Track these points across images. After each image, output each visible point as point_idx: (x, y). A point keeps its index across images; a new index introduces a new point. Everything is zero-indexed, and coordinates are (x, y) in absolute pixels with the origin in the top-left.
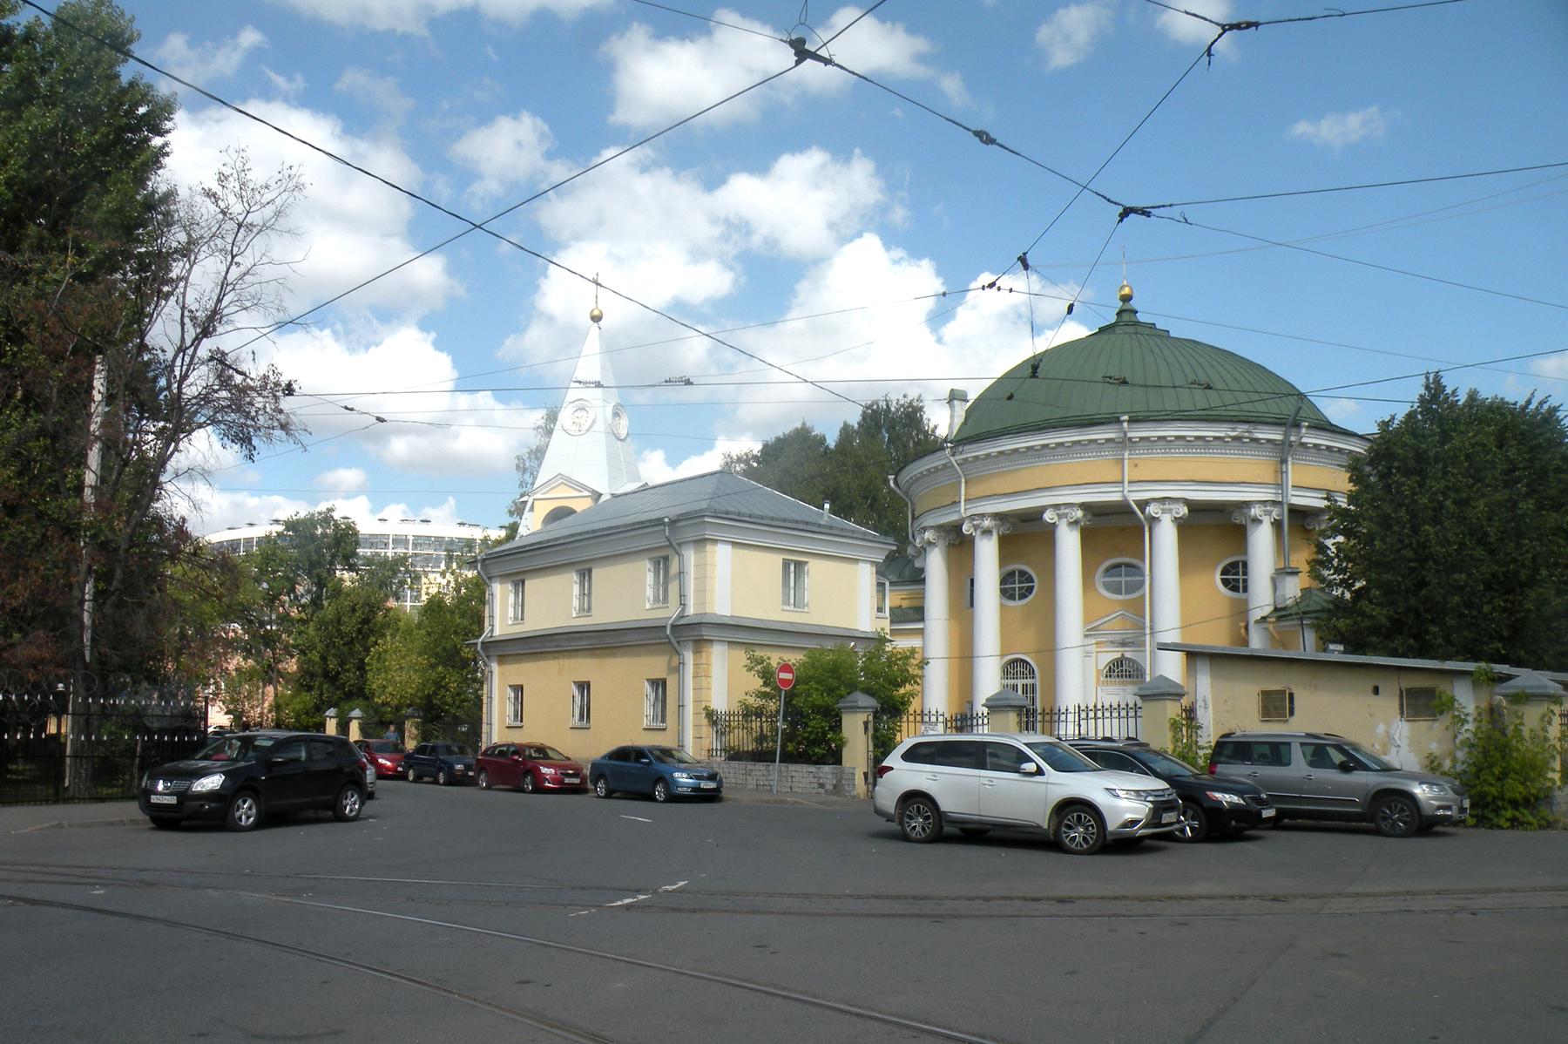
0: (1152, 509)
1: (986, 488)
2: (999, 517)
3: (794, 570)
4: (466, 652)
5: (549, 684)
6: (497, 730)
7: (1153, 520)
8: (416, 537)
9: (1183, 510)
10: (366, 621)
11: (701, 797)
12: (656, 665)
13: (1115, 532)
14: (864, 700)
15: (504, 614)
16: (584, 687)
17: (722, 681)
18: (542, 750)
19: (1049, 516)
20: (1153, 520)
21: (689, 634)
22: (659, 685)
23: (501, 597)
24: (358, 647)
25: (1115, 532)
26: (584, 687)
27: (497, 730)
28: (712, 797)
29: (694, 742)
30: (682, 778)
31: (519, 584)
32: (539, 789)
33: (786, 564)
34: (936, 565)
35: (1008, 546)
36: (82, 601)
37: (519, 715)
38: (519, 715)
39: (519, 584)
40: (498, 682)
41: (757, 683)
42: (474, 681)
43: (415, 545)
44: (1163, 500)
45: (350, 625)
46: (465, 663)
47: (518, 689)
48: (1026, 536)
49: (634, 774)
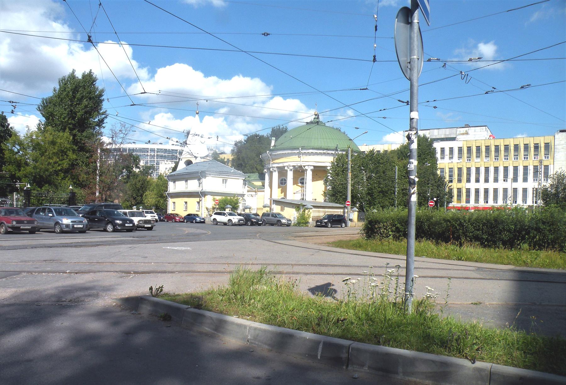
0: (306, 167)
1: (275, 161)
2: (277, 167)
3: (225, 181)
4: (164, 195)
5: (180, 202)
6: (170, 211)
7: (306, 170)
8: (158, 149)
9: (312, 168)
10: (143, 184)
11: (201, 222)
12: (198, 199)
13: (299, 173)
14: (229, 206)
15: (173, 187)
16: (186, 203)
17: (209, 202)
18: (177, 214)
19: (286, 168)
20: (306, 170)
21: (203, 194)
22: (198, 203)
23: (171, 184)
24: (140, 191)
25: (299, 173)
26: (186, 203)
27: (170, 211)
28: (204, 222)
29: (203, 214)
30: (198, 219)
31: (174, 182)
32: (176, 222)
33: (223, 180)
34: (267, 177)
35: (279, 173)
36: (95, 184)
37: (174, 208)
38: (174, 208)
39: (174, 182)
40: (170, 201)
41: (214, 203)
42: (165, 200)
43: (157, 152)
44: (308, 166)
45: (139, 185)
46: (164, 197)
47: (174, 203)
48: (282, 172)
49: (191, 218)
